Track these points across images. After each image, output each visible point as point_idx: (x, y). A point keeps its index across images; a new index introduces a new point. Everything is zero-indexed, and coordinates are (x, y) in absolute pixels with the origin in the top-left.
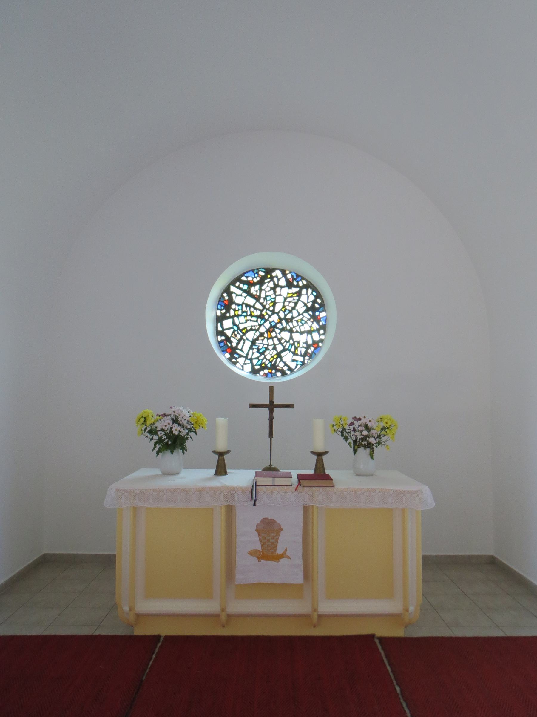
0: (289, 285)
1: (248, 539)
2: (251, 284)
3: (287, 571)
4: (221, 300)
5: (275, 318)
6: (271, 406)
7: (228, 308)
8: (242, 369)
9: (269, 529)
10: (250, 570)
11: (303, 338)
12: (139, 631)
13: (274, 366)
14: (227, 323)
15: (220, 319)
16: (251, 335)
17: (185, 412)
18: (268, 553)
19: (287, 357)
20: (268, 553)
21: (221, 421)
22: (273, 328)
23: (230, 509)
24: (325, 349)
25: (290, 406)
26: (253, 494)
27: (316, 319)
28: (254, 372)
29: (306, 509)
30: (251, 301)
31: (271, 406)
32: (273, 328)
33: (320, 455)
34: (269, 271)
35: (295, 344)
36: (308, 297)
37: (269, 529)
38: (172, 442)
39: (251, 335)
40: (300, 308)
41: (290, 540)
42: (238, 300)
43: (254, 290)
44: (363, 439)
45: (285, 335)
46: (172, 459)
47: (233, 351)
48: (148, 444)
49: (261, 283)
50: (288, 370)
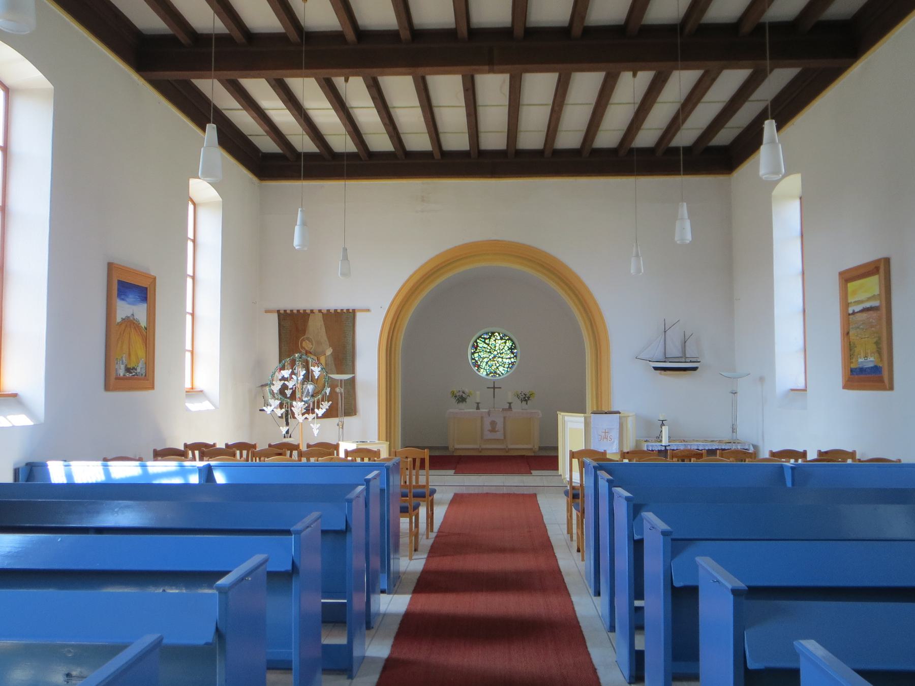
0: (501, 339)
1: (487, 426)
2: (485, 339)
3: (499, 435)
4: (473, 345)
5: (495, 353)
6: (494, 388)
7: (476, 349)
8: (483, 373)
9: (493, 423)
10: (488, 435)
11: (508, 361)
12: (455, 454)
13: (495, 373)
14: (476, 355)
15: (473, 354)
16: (486, 360)
17: (467, 390)
18: (493, 430)
19: (501, 369)
20: (493, 430)
21: (478, 393)
22: (495, 357)
23: (482, 418)
24: (516, 364)
25: (368, 310)
26: (489, 413)
27: (512, 353)
28: (487, 375)
29: (505, 418)
30: (485, 346)
31: (494, 388)
32: (495, 357)
33: (510, 404)
34: (493, 333)
35: (504, 363)
36: (509, 344)
37: (493, 423)
38: (462, 399)
39: (486, 360)
40: (506, 348)
41: (500, 426)
42: (480, 345)
43: (487, 341)
44: (526, 399)
45: (500, 360)
46: (462, 405)
47: (479, 366)
48: (454, 400)
49: (490, 338)
50: (432, 530)
